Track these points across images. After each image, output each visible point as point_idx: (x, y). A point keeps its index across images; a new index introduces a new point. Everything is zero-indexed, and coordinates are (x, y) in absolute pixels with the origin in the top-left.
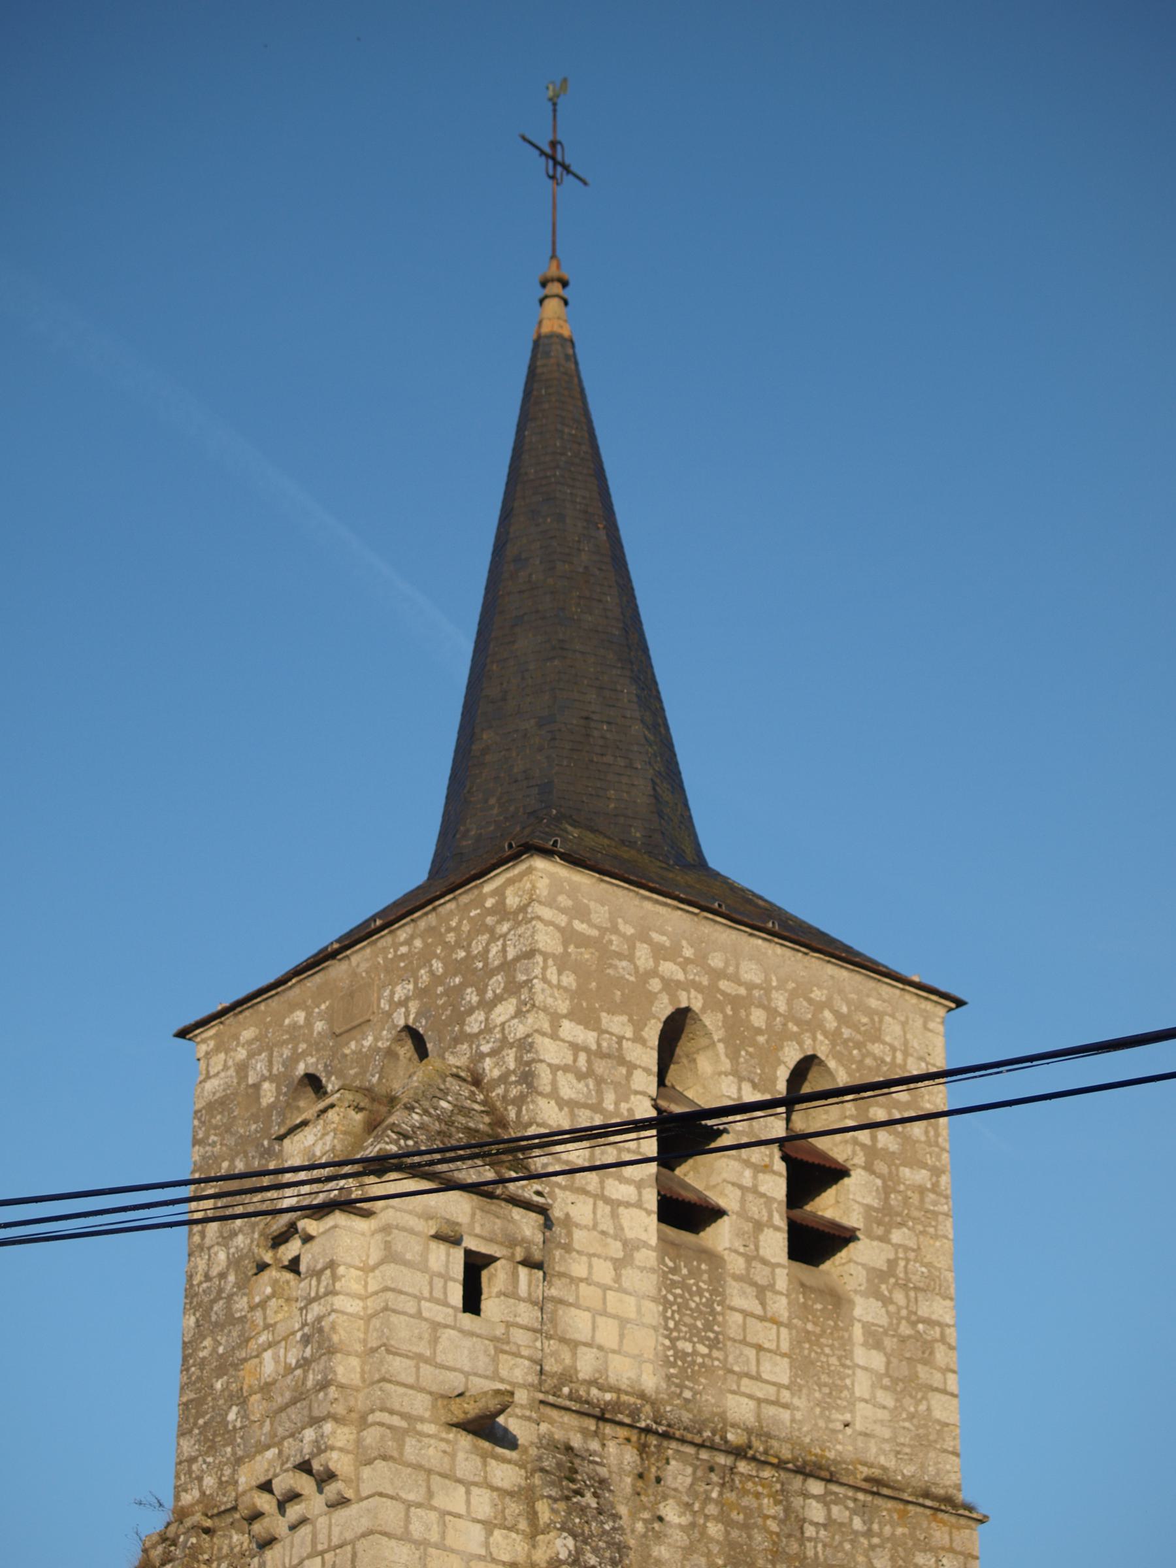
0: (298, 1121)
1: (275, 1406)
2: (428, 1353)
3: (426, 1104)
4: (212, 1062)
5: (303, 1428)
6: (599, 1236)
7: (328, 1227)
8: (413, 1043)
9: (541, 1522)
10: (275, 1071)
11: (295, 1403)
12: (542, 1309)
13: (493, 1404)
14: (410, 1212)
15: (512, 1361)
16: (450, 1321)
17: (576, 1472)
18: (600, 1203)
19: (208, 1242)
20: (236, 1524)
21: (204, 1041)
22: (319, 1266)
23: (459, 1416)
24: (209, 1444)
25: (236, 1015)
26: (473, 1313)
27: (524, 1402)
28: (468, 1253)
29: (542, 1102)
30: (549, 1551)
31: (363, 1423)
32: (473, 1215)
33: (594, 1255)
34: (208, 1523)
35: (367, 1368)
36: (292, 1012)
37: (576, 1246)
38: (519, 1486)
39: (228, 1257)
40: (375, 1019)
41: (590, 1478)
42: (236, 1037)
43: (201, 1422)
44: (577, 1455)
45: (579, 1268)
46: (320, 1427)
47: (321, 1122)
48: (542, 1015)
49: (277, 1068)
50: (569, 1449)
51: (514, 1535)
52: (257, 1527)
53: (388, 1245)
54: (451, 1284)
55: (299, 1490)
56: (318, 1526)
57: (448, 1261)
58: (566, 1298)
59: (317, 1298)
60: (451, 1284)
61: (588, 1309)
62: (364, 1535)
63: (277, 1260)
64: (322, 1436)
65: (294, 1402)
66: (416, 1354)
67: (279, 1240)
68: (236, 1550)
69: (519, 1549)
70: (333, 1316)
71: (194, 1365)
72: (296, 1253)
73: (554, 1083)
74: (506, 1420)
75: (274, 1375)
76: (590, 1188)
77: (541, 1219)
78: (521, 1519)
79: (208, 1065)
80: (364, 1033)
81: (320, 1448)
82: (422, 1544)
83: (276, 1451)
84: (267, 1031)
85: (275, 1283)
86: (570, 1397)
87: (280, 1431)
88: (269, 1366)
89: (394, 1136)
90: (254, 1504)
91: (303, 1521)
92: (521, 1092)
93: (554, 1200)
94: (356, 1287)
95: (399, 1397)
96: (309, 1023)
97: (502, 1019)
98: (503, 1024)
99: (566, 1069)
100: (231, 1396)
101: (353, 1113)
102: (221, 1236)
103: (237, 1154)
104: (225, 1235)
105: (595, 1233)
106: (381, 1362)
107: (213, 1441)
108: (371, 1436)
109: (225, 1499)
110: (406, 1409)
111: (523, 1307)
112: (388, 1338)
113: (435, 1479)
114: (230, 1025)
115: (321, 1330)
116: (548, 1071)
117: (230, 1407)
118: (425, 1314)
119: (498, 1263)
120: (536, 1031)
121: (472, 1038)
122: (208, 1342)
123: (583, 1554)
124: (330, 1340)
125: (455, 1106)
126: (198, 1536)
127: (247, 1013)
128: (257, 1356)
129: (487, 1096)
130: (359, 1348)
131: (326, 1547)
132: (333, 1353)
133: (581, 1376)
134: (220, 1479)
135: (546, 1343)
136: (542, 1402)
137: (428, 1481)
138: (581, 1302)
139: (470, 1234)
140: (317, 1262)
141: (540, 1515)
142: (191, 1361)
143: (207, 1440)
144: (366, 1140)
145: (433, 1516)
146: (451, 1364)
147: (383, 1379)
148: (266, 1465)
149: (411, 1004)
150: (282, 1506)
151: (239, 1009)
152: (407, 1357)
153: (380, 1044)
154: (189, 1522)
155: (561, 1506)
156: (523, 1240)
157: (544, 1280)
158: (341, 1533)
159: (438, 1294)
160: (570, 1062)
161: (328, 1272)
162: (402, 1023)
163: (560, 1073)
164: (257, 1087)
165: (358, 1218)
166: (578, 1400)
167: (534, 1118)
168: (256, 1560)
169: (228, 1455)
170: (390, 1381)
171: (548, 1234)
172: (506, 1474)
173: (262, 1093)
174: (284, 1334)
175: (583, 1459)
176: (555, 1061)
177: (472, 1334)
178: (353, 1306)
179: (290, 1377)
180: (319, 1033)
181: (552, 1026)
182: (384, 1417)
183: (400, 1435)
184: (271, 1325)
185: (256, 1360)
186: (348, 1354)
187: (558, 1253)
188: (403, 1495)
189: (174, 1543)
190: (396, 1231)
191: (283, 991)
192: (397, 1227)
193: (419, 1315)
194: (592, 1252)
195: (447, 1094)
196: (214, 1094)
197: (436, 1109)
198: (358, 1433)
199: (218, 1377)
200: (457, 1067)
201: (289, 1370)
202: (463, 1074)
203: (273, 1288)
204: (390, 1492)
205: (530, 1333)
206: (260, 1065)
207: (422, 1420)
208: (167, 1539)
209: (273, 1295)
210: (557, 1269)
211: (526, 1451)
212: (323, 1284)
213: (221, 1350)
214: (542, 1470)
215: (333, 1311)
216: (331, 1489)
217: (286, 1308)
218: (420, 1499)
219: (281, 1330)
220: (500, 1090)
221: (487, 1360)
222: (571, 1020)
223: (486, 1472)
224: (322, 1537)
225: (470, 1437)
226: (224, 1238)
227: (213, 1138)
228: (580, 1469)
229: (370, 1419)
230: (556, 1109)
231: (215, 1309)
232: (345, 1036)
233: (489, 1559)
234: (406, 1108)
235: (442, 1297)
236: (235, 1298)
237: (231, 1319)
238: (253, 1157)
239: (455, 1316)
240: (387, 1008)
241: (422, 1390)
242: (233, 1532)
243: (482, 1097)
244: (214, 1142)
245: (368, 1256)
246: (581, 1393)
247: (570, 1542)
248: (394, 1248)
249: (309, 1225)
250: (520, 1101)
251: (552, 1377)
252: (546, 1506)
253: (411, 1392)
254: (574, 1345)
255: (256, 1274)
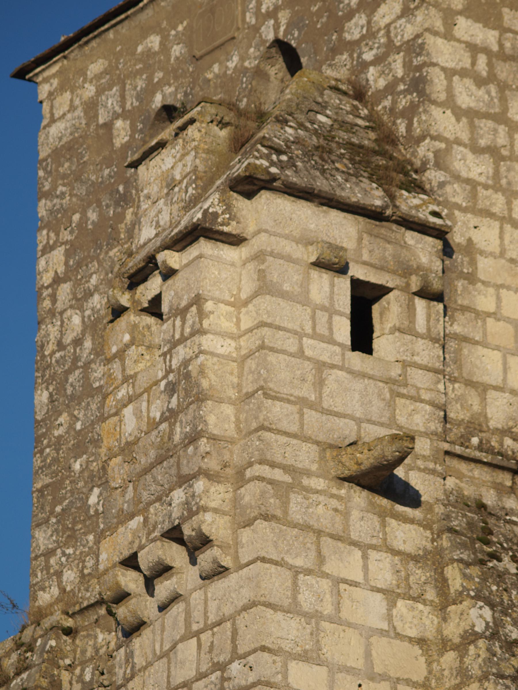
0: (154, 143)
1: (138, 468)
2: (313, 398)
3: (301, 118)
4: (56, 103)
5: (171, 490)
6: (507, 264)
7: (191, 258)
8: (285, 61)
9: (452, 591)
10: (128, 106)
11: (161, 463)
12: (444, 348)
13: (390, 452)
14: (287, 237)
15: (411, 406)
16: (337, 360)
17: (491, 533)
18: (508, 227)
19: (59, 306)
20: (102, 622)
21: (46, 80)
22: (184, 303)
23: (351, 468)
24: (68, 533)
25: (81, 46)
26: (363, 351)
27: (427, 453)
28: (356, 283)
29: (436, 112)
30: (463, 624)
31: (240, 479)
32: (360, 240)
33: (502, 286)
34: (69, 623)
35: (242, 417)
36: (145, 38)
37: (481, 276)
38: (425, 549)
39: (83, 321)
40: (239, 36)
41: (507, 540)
42: (83, 72)
43: (58, 509)
44: (490, 514)
45: (485, 302)
46: (191, 486)
47: (180, 141)
48: (433, 11)
49: (131, 102)
50: (481, 506)
51: (420, 606)
52: (122, 611)
53: (262, 274)
54: (336, 319)
55: (168, 562)
56: (192, 602)
57: (332, 292)
58: (471, 335)
59: (183, 340)
60: (336, 319)
61: (497, 348)
62: (245, 608)
63: (134, 301)
64: (193, 496)
65: (159, 461)
66: (298, 398)
67: (136, 279)
68: (102, 651)
69: (428, 622)
70: (202, 358)
71: (49, 446)
72: (157, 292)
73: (449, 90)
74: (407, 473)
75: (136, 433)
76: (495, 210)
77: (439, 244)
78: (428, 588)
79: (52, 107)
80: (228, 54)
81: (192, 510)
82: (313, 617)
83: (141, 519)
84: (118, 63)
85: (133, 328)
86: (480, 448)
87: (145, 496)
88: (130, 423)
89: (265, 151)
90: (117, 584)
91: (175, 598)
92: (412, 102)
93: (455, 223)
94: (227, 325)
95: (279, 447)
96: (165, 48)
97: (387, 20)
98: (388, 26)
99: (463, 73)
100: (92, 477)
101: (216, 128)
102: (75, 298)
103: (89, 205)
104: (79, 296)
105: (503, 261)
106: (259, 408)
107: (73, 529)
108: (250, 493)
109: (88, 594)
110: (290, 461)
111: (421, 344)
112: (265, 381)
113: (326, 541)
114: (75, 60)
115: (188, 376)
116: (443, 76)
117: (91, 490)
118: (308, 353)
119: (391, 295)
120: (427, 30)
121: (352, 46)
122: (63, 418)
123: (503, 627)
124: (198, 385)
125: (335, 121)
126: (58, 638)
127: (94, 44)
128: (116, 414)
129: (372, 110)
130: (232, 394)
131: (201, 626)
132: (202, 401)
133: (492, 424)
134: (82, 571)
135: (450, 386)
136: (447, 453)
137: (318, 545)
138: (490, 339)
139: (357, 262)
140: (181, 299)
141: (450, 582)
142: (45, 442)
143: (66, 528)
144: (232, 159)
145: (325, 584)
146: (339, 409)
147: (262, 428)
148: (130, 537)
149: (280, 15)
150: (149, 585)
151: (85, 39)
152: (289, 401)
153: (247, 64)
154: (47, 623)
155: (475, 571)
156: (419, 268)
157: (445, 315)
158: (219, 608)
159: (322, 329)
160: (468, 66)
161: (194, 309)
162: (271, 37)
163: (456, 78)
164: (108, 126)
165: (226, 247)
166: (490, 450)
167: (428, 130)
168: (122, 651)
169: (91, 544)
170: (270, 430)
171: (447, 262)
172: (408, 534)
173: (115, 133)
174: (146, 385)
175: (498, 518)
176: (450, 65)
177: (363, 375)
178: (224, 347)
179: (155, 433)
180: (177, 58)
181: (445, 23)
182: (265, 471)
183: (282, 491)
184: (131, 377)
185: (116, 418)
186: (221, 401)
187: (460, 284)
188: (290, 560)
189: (31, 648)
190: (270, 259)
191: (135, 14)
192: (272, 254)
193: (300, 354)
194: (499, 282)
195: (326, 108)
196: (60, 139)
197: (312, 123)
198: (235, 491)
199: (76, 458)
200: (336, 80)
201: (154, 425)
202: (344, 87)
203: (132, 334)
204: (274, 557)
205: (431, 374)
206: (111, 101)
207: (308, 473)
208: (22, 645)
209: (132, 342)
210: (459, 302)
211: (430, 509)
212: (189, 323)
213: (78, 426)
214: (451, 530)
215: (201, 352)
216: (206, 558)
217: (148, 357)
218: (309, 565)
219: (142, 382)
220: (387, 103)
221: (382, 404)
222: (467, 17)
223: (385, 534)
224: (197, 615)
225: (365, 493)
226: (78, 300)
227: (61, 189)
228: (495, 530)
229: (249, 473)
230: (453, 119)
231: (70, 380)
232: (208, 58)
233: (392, 634)
234: (278, 120)
235: (326, 333)
236: (93, 366)
237: (89, 390)
238: (108, 206)
239: (343, 355)
240: (253, 21)
241: (307, 439)
242: (98, 630)
243: (366, 111)
244: (63, 193)
245: (239, 289)
246: (493, 444)
247: (487, 613)
248: (268, 278)
249: (171, 258)
250: (410, 112)
251: (459, 425)
252: (457, 571)
253: (294, 441)
254: (482, 389)
255: (112, 321)
